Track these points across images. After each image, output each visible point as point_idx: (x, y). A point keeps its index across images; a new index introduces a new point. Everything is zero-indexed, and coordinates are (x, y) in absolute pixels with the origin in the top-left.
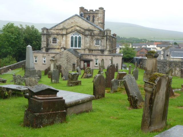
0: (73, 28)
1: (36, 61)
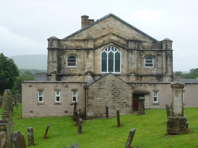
1: (41, 99)
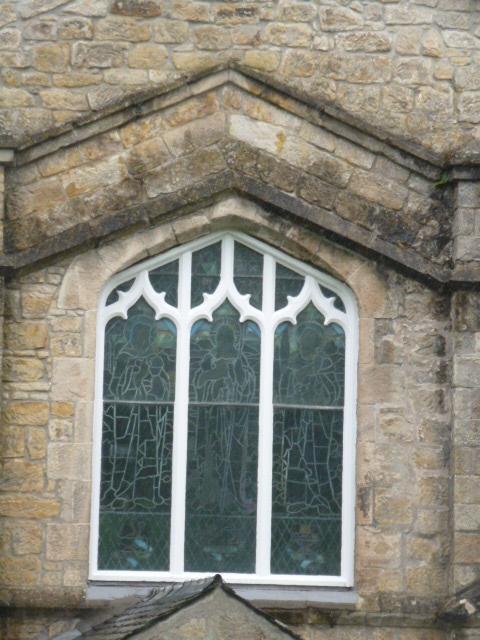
0: (161, 135)
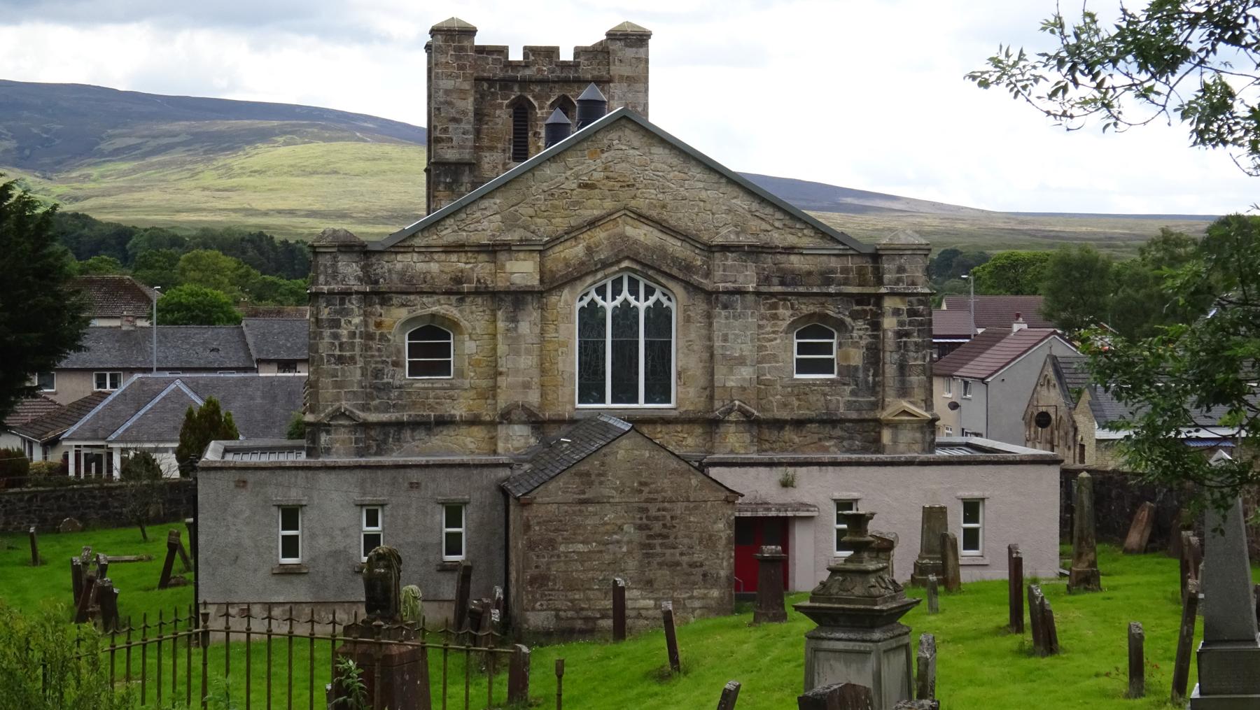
1: (290, 547)
